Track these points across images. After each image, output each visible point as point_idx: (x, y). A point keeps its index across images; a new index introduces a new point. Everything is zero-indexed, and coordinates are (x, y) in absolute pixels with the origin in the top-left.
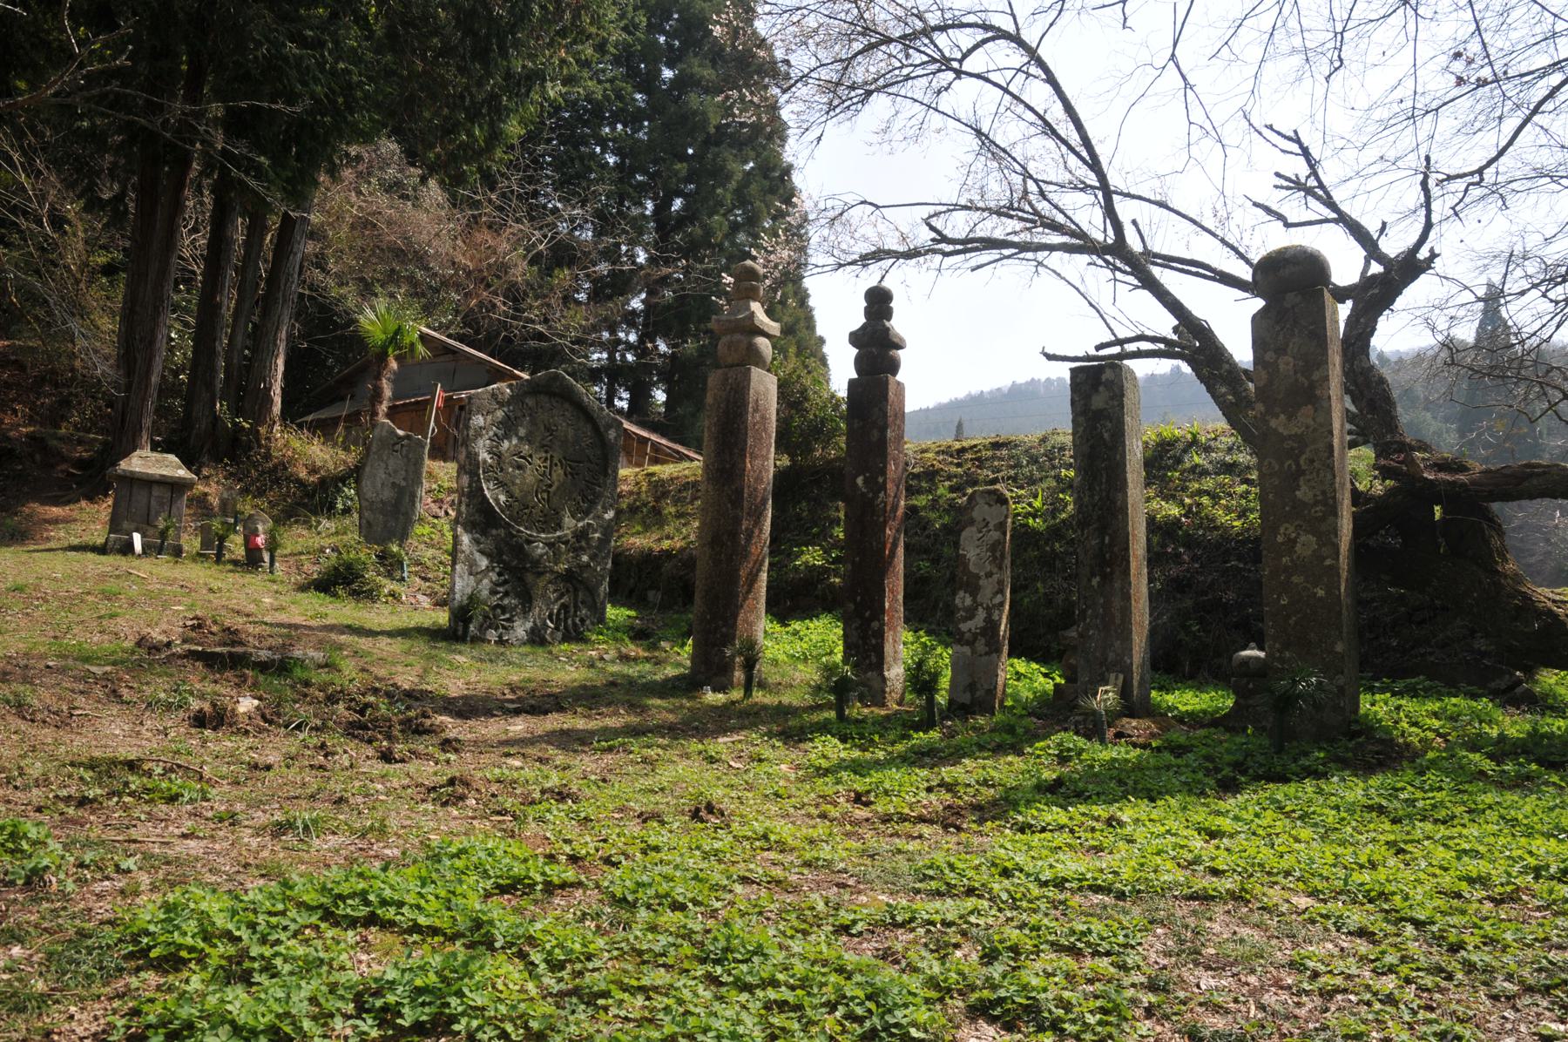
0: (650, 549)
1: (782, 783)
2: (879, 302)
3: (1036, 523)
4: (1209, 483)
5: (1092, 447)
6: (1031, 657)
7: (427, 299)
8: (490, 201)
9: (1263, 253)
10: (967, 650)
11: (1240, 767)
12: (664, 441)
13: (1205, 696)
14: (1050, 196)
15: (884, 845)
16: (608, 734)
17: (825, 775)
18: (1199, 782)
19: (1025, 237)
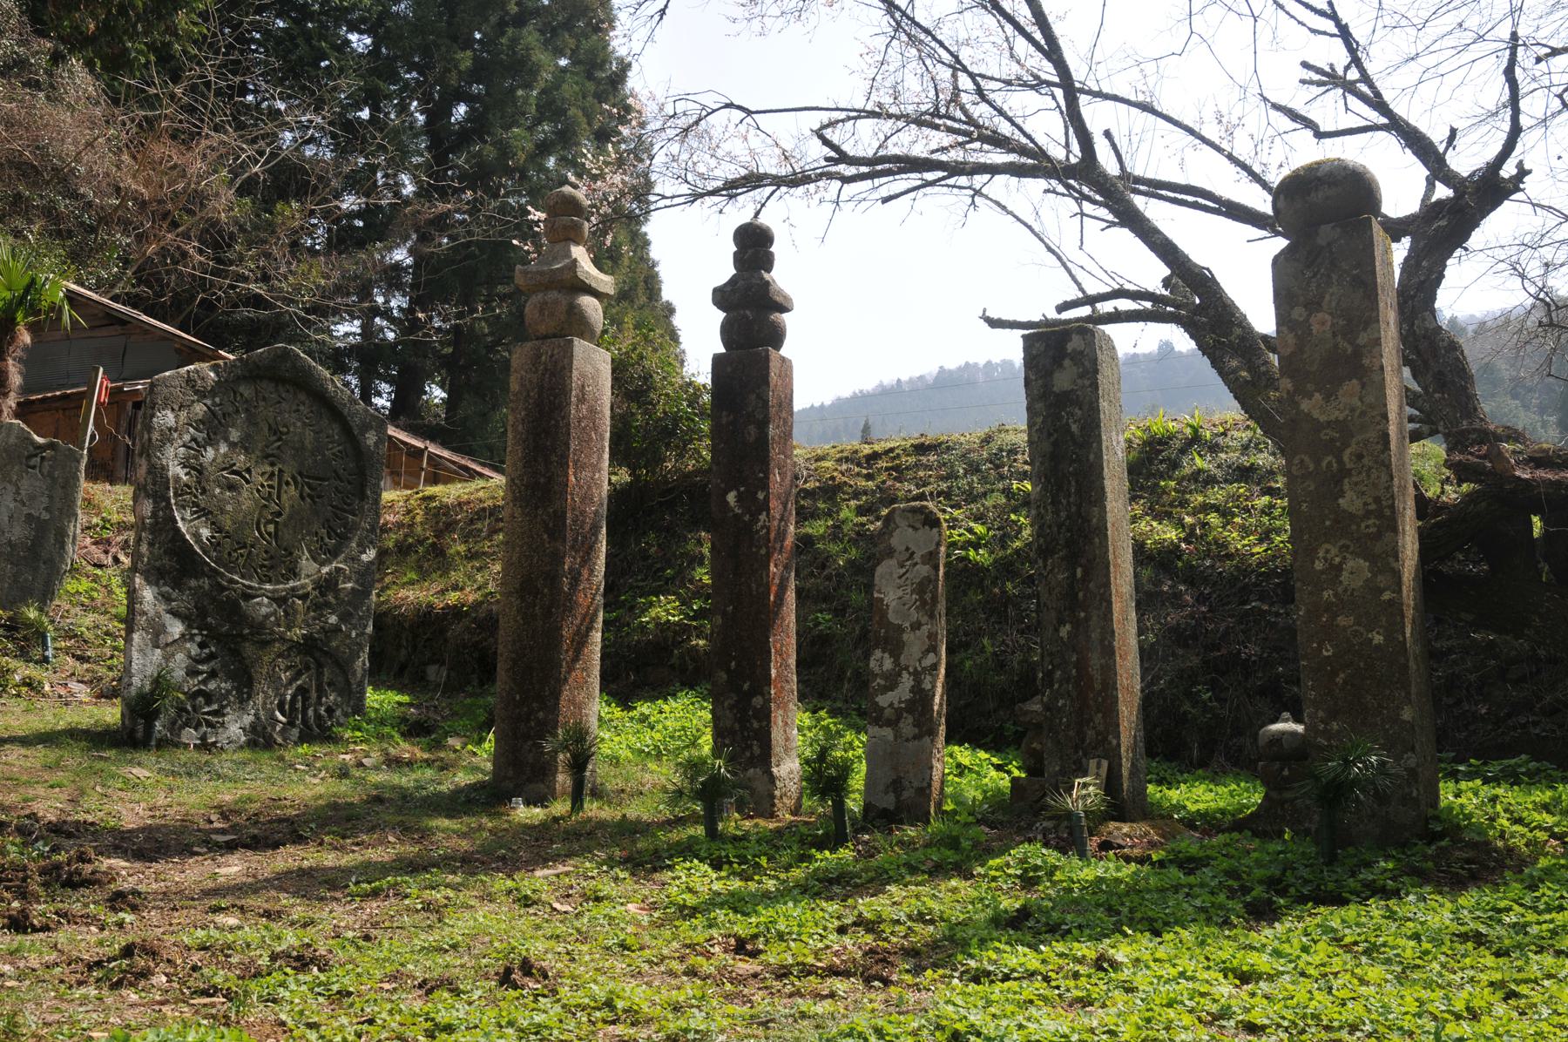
0: (430, 606)
1: (630, 929)
2: (754, 245)
3: (981, 556)
4: (1217, 495)
5: (1055, 444)
6: (976, 742)
7: (77, 240)
8: (172, 96)
9: (1286, 172)
10: (888, 733)
11: (1276, 885)
12: (446, 454)
13: (1221, 790)
14: (991, 96)
15: (782, 1008)
16: (369, 871)
17: (692, 916)
18: (1221, 907)
19: (956, 155)
